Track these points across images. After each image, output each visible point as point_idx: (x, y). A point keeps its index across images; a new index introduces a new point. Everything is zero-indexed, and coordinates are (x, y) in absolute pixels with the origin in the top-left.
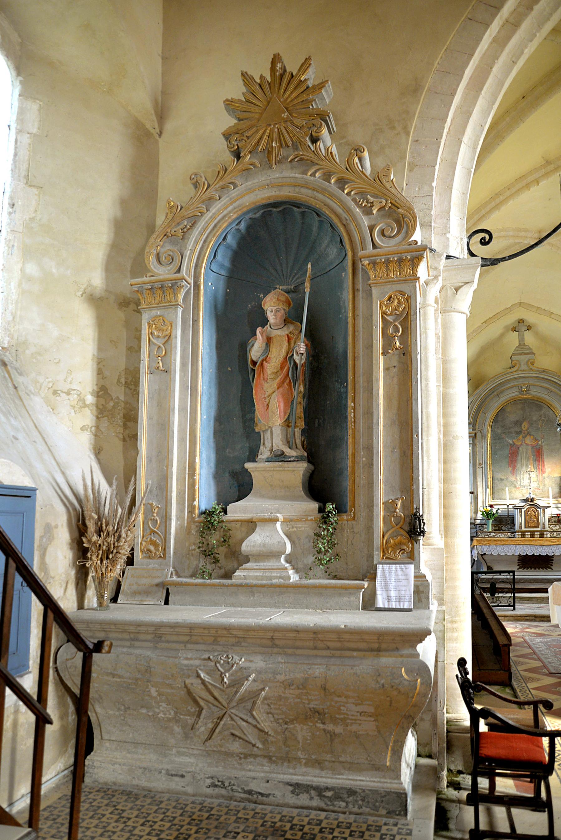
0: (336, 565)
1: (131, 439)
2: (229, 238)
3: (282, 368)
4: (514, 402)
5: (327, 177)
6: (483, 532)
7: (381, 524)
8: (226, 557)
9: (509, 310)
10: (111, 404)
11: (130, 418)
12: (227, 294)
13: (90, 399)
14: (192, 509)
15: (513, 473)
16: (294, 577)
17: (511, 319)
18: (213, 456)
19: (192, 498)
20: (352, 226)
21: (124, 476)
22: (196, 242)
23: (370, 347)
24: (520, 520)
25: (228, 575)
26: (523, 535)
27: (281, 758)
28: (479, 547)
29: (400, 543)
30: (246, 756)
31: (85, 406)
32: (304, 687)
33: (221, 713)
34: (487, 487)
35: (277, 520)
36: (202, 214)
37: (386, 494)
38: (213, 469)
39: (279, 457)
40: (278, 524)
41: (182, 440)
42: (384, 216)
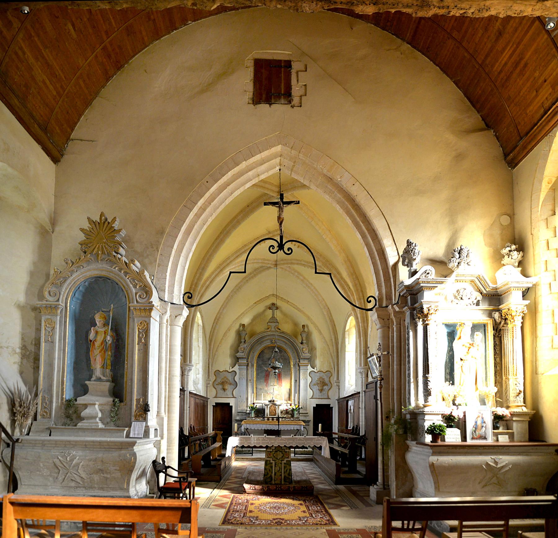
0: (118, 422)
1: (36, 368)
2: (81, 288)
3: (102, 344)
4: (268, 348)
5: (120, 270)
6: (249, 417)
7: (135, 407)
8: (76, 418)
9: (268, 297)
10: (28, 353)
11: (37, 359)
12: (80, 310)
13: (18, 350)
14: (62, 398)
15: (266, 386)
16: (101, 426)
17: (268, 302)
18: (72, 378)
19: (62, 394)
20: (129, 292)
21: (33, 384)
22: (66, 289)
23: (133, 341)
24: (267, 411)
25: (76, 426)
26: (268, 419)
27: (89, 487)
28: (245, 425)
29: (141, 414)
30: (77, 487)
31: (16, 353)
32: (96, 461)
33: (66, 472)
34: (253, 392)
35: (95, 404)
36: (69, 277)
37: (137, 396)
38: (72, 383)
39: (99, 379)
40: (97, 406)
41: (59, 371)
42: (141, 289)
